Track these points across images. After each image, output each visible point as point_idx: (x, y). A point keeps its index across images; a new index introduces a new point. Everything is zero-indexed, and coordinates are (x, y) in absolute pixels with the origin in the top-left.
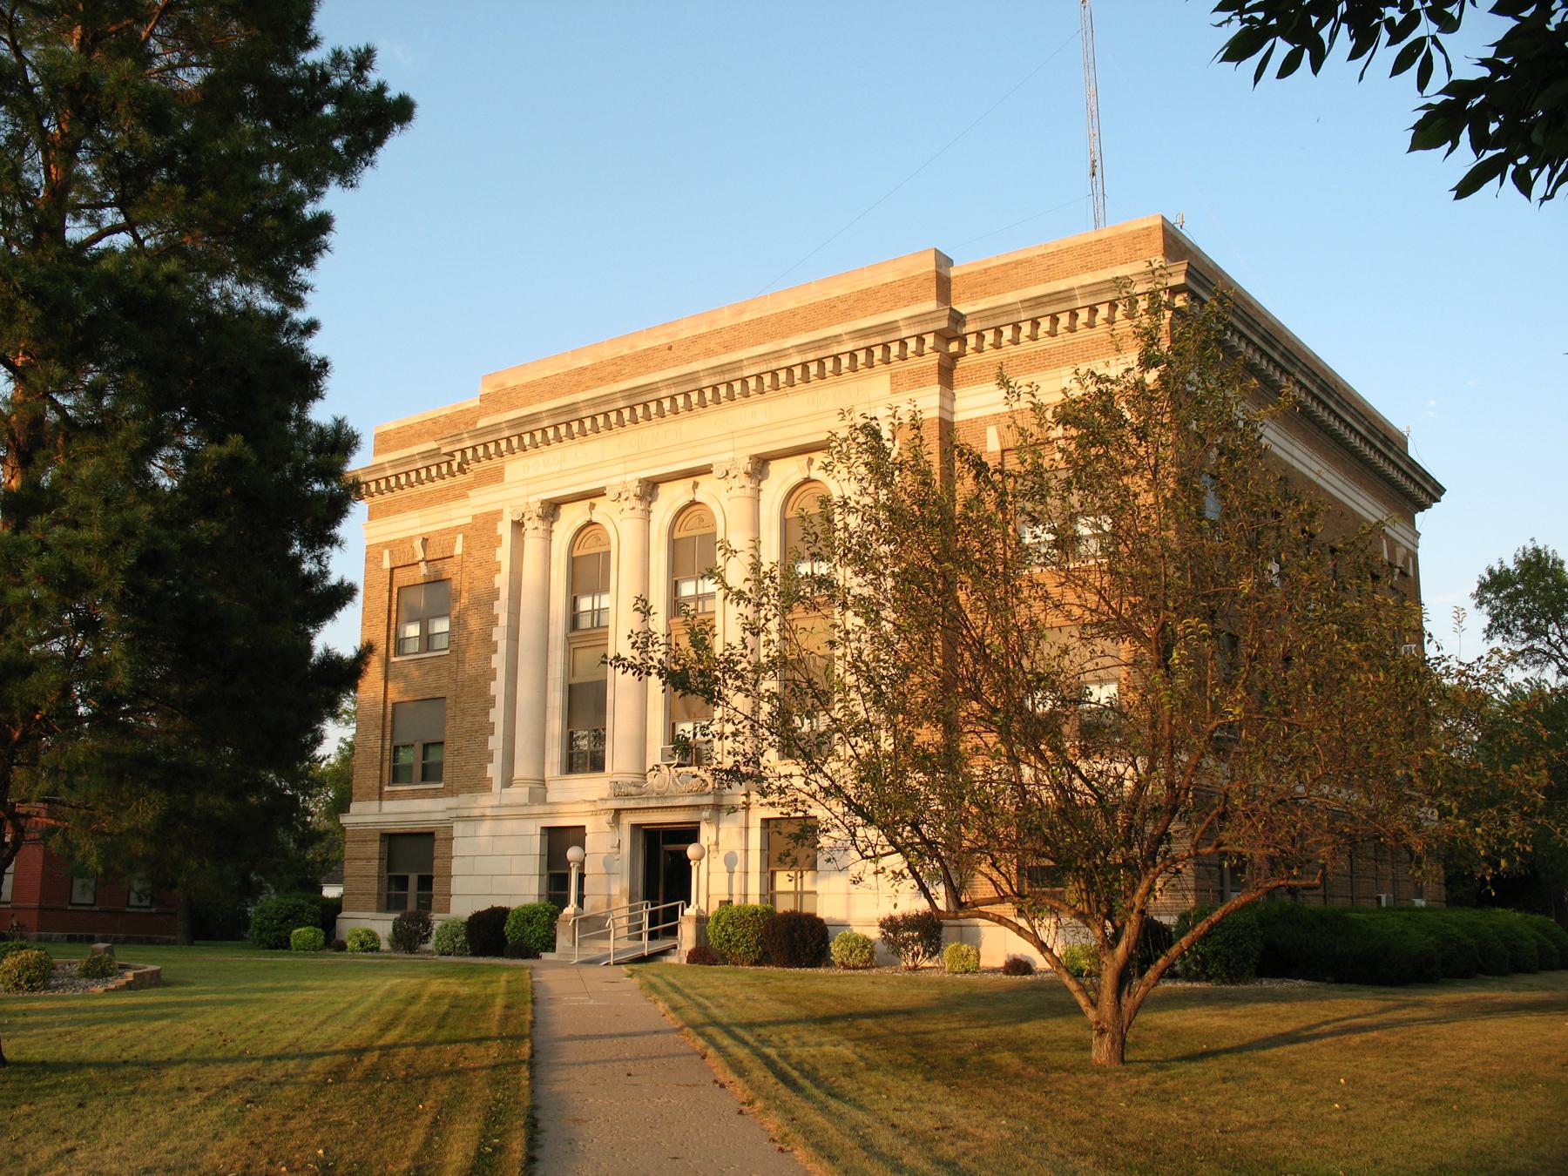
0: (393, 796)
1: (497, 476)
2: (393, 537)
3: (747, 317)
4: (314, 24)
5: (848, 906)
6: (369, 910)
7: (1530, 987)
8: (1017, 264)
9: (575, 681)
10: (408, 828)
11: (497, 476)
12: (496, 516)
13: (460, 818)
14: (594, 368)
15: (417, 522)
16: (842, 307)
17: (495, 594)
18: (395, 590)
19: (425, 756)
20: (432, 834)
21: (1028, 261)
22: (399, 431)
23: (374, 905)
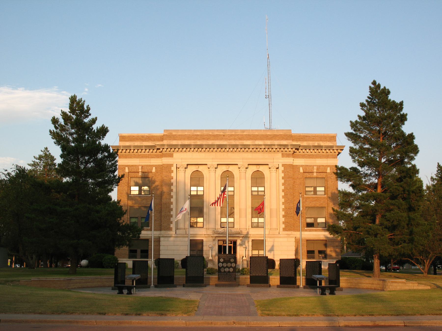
0: (306, 231)
1: (171, 156)
2: (129, 164)
3: (245, 133)
4: (397, 102)
5: (274, 257)
6: (125, 258)
7: (90, 290)
8: (307, 136)
9: (192, 206)
10: (317, 238)
11: (171, 156)
12: (171, 165)
13: (163, 237)
14: (201, 135)
15: (138, 162)
16: (270, 137)
17: (172, 184)
18: (129, 178)
19: (130, 220)
20: (148, 240)
21: (309, 136)
22: (129, 136)
23: (127, 257)
